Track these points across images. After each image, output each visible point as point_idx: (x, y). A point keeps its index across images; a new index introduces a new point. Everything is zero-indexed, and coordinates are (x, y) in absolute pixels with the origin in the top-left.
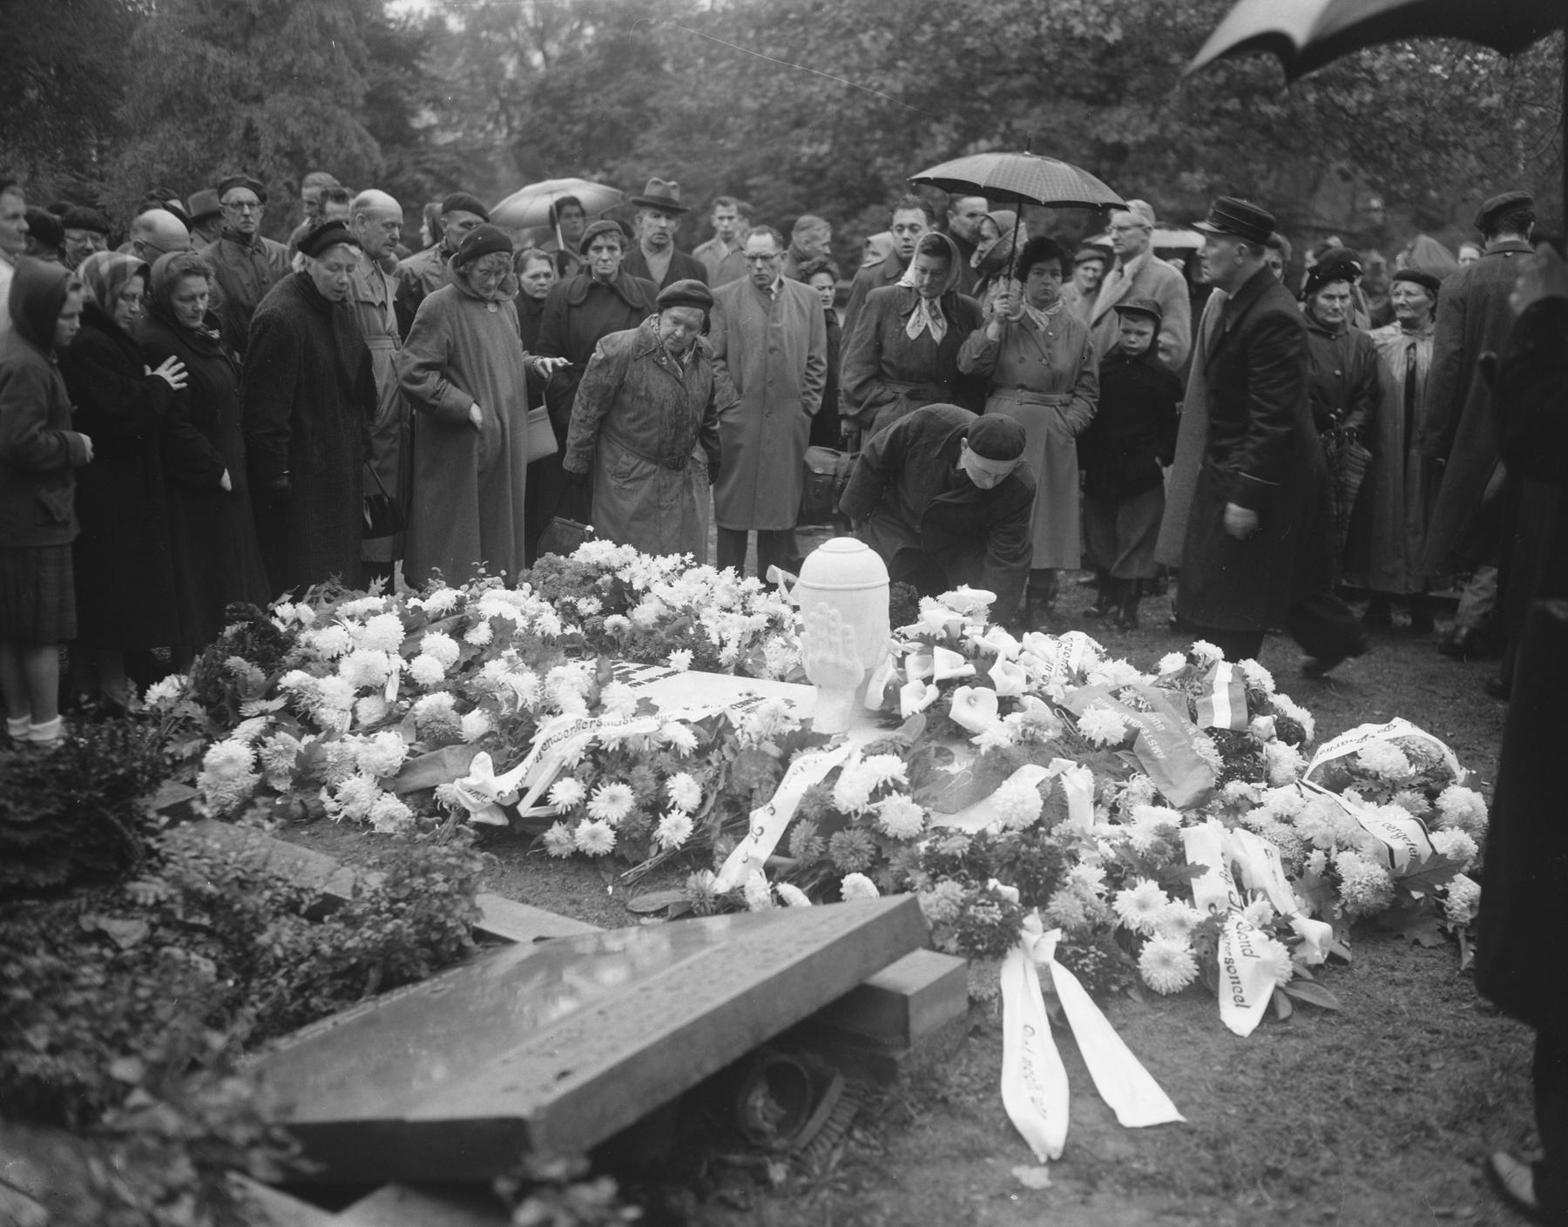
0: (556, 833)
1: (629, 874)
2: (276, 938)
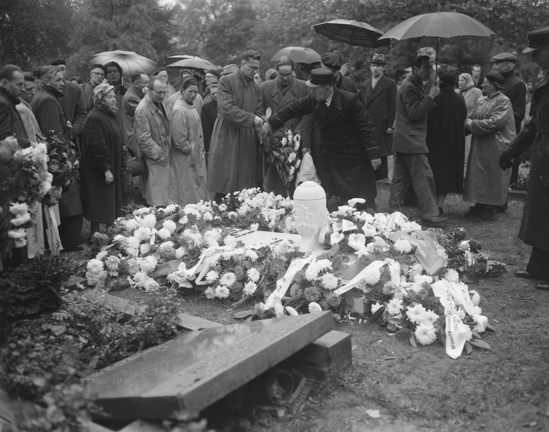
0: (209, 290)
1: (235, 305)
2: (107, 331)
